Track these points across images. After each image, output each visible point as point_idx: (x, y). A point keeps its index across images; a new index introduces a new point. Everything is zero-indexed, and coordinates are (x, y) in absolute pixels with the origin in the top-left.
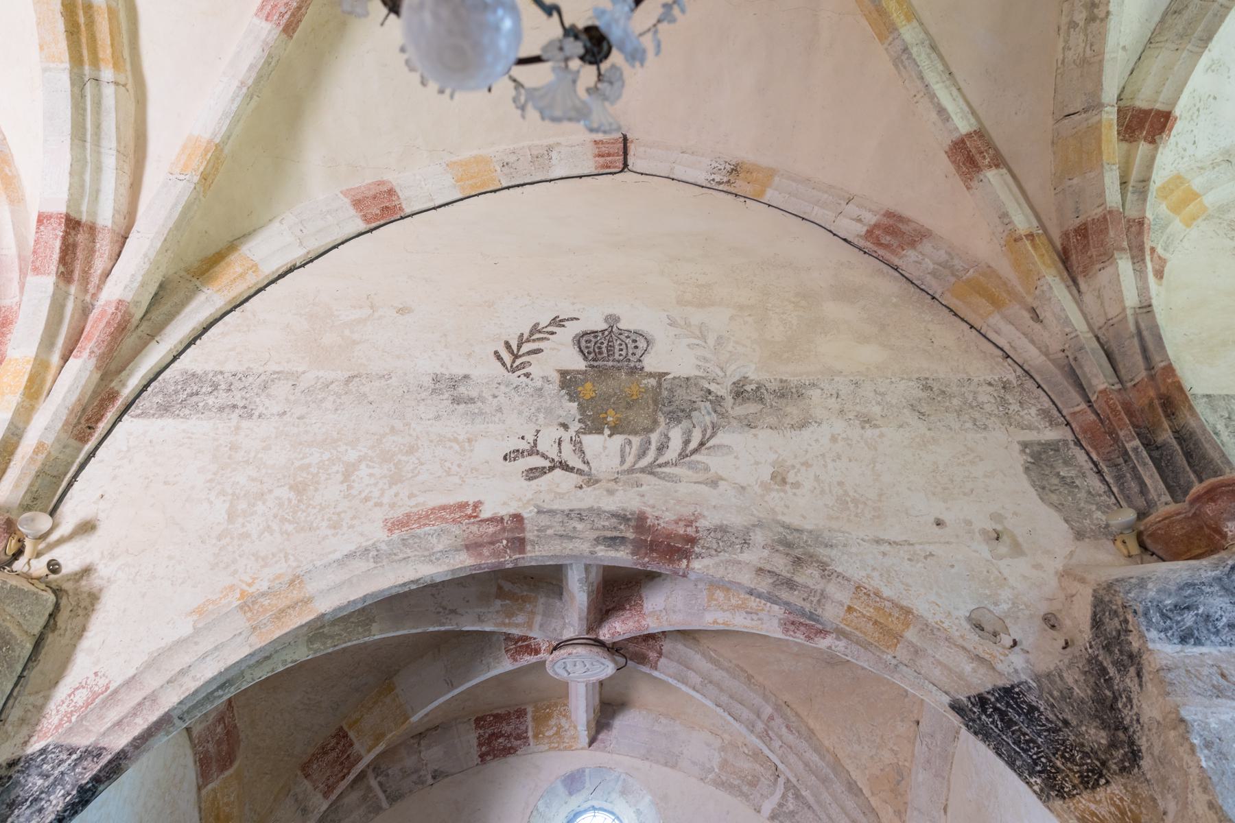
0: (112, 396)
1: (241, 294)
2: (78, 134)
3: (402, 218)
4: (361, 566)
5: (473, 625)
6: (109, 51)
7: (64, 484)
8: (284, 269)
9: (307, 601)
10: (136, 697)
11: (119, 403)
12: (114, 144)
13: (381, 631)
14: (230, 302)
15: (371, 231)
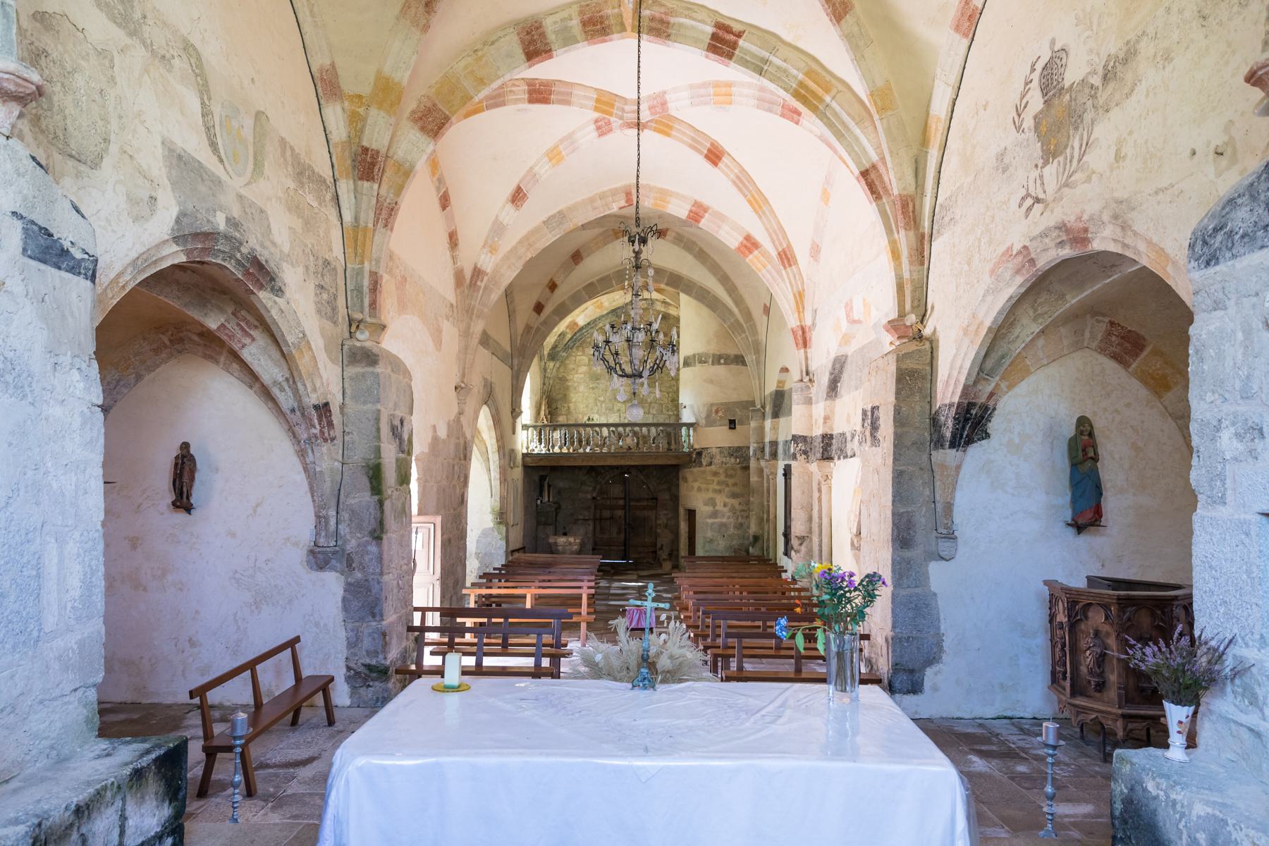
0: (923, 236)
1: (941, 141)
2: (839, 135)
3: (981, 14)
4: (989, 298)
5: (1132, 267)
6: (820, 90)
7: (925, 289)
8: (950, 107)
9: (982, 323)
10: (952, 382)
11: (927, 238)
12: (853, 124)
13: (1073, 298)
14: (939, 149)
15: (973, 39)
